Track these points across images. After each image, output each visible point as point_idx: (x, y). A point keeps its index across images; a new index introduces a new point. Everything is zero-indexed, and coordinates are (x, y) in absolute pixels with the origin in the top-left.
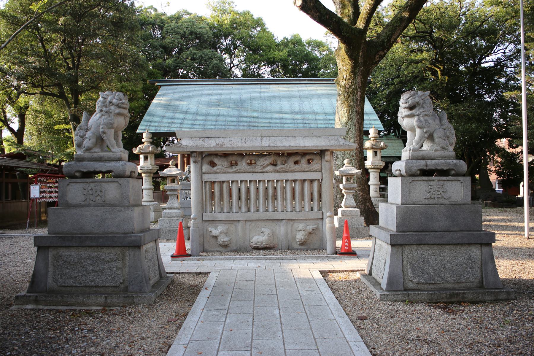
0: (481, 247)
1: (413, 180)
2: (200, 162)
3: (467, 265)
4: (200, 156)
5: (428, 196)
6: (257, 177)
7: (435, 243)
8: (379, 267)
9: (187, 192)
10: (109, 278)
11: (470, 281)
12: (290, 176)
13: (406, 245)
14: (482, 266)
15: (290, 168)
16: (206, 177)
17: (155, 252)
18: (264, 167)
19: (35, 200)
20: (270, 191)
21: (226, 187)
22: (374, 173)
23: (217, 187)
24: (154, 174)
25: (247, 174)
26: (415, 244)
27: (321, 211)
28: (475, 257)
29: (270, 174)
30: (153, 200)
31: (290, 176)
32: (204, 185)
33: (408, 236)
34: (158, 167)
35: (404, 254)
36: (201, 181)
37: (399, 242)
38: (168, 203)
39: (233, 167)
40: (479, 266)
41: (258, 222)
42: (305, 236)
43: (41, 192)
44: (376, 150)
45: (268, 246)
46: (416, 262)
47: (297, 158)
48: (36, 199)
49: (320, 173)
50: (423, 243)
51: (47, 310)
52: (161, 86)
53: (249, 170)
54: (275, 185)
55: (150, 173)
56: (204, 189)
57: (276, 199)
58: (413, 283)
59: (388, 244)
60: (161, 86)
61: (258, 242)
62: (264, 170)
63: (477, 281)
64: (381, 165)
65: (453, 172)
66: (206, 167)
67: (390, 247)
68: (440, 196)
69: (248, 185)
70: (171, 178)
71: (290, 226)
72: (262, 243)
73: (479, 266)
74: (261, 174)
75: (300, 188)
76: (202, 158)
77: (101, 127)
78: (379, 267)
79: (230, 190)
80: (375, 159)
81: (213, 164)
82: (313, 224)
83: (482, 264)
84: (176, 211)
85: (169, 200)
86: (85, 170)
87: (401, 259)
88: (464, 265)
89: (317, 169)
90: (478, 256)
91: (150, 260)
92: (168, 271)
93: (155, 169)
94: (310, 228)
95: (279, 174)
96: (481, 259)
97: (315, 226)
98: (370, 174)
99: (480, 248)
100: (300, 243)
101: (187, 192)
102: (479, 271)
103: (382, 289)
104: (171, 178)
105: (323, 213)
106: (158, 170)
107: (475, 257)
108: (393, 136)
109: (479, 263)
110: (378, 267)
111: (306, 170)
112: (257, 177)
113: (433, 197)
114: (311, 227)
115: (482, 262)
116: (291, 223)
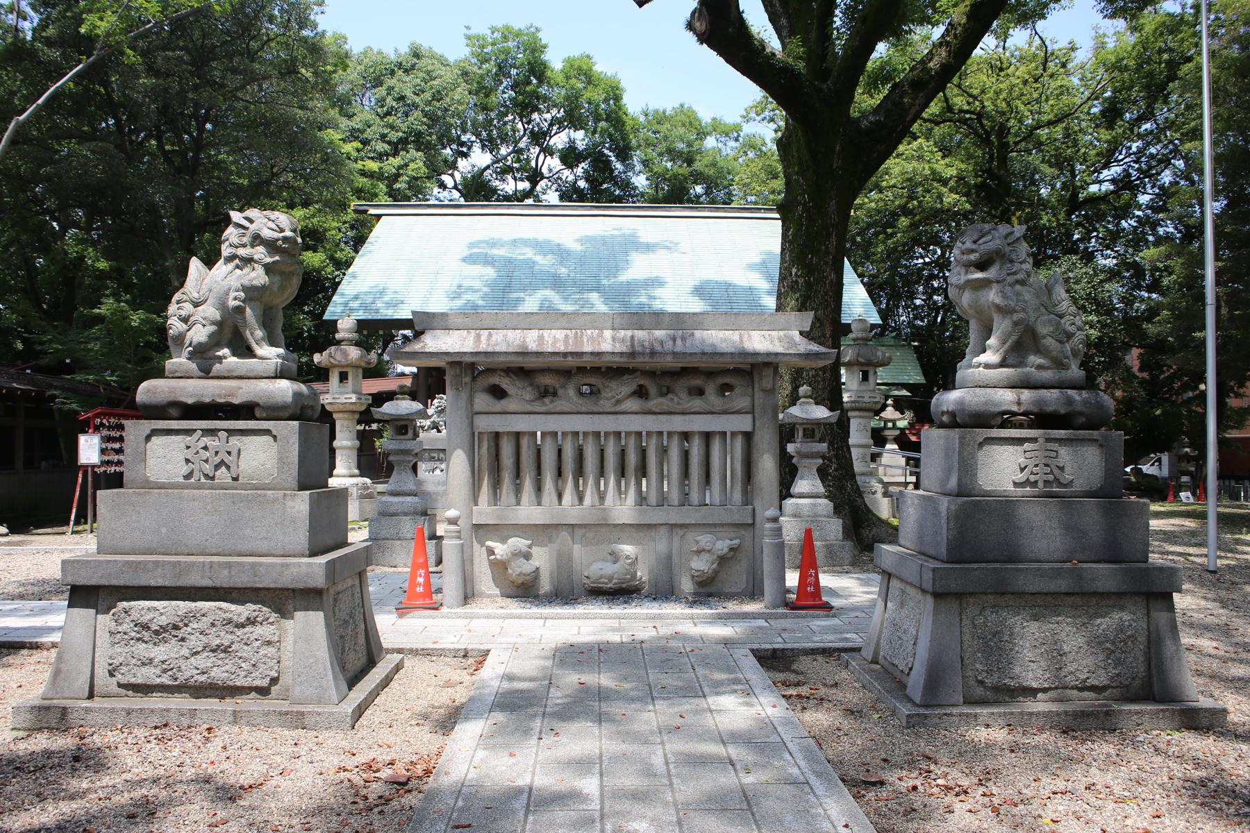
0: (1147, 600)
1: (986, 439)
2: (469, 386)
3: (1113, 643)
4: (469, 372)
5: (1020, 477)
6: (606, 424)
7: (1038, 590)
8: (901, 645)
9: (436, 455)
10: (243, 665)
11: (1121, 683)
12: (678, 424)
13: (971, 594)
14: (1149, 648)
15: (679, 403)
16: (487, 424)
17: (358, 601)
18: (618, 402)
19: (90, 469)
20: (632, 459)
21: (529, 447)
22: (859, 420)
23: (507, 449)
24: (361, 413)
25: (579, 416)
26: (992, 593)
27: (750, 507)
28: (1134, 624)
29: (633, 417)
30: (357, 471)
31: (678, 424)
32: (476, 439)
33: (977, 573)
34: (370, 397)
35: (964, 617)
36: (467, 432)
37: (954, 586)
38: (391, 480)
39: (546, 400)
40: (1142, 647)
41: (603, 530)
42: (713, 564)
43: (103, 451)
44: (865, 368)
45: (624, 586)
46: (994, 636)
47: (697, 382)
48: (93, 466)
49: (750, 416)
50: (1011, 590)
51: (123, 709)
52: (379, 217)
53: (584, 409)
54: (644, 444)
55: (353, 412)
56: (476, 450)
57: (644, 475)
58: (985, 687)
59: (924, 591)
60: (379, 217)
61: (601, 577)
62: (618, 409)
63: (1137, 682)
64: (876, 403)
65: (1082, 420)
66: (483, 401)
67: (930, 600)
68: (1051, 477)
69: (581, 442)
70: (211, 375)
71: (676, 540)
72: (610, 579)
73: (1142, 647)
74: (611, 417)
75: (702, 452)
76: (474, 378)
77: (233, 295)
78: (901, 645)
79: (539, 452)
80: (863, 388)
81: (498, 393)
82: (732, 535)
83: (1149, 642)
84: (409, 499)
85: (394, 473)
86: (190, 401)
87: (958, 629)
88: (1108, 645)
89: (742, 409)
90: (1141, 623)
91: (346, 622)
92: (390, 647)
93: (363, 401)
94: (723, 546)
95: (654, 417)
96: (1149, 631)
97: (737, 541)
98: (852, 421)
99: (1145, 602)
100: (701, 580)
101: (436, 455)
102: (1142, 659)
103: (910, 700)
104: (211, 375)
105: (754, 510)
106: (370, 405)
107: (1134, 624)
108: (893, 337)
109: (1142, 639)
110: (898, 646)
111: (717, 409)
112: (606, 424)
113: (1033, 478)
114: (728, 542)
115: (1149, 637)
116: (680, 532)
